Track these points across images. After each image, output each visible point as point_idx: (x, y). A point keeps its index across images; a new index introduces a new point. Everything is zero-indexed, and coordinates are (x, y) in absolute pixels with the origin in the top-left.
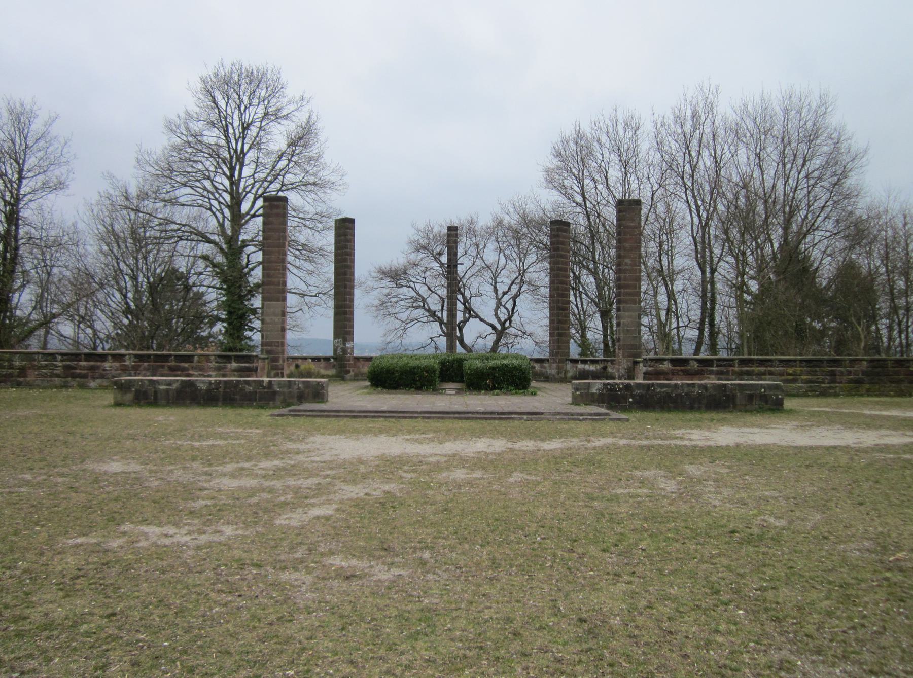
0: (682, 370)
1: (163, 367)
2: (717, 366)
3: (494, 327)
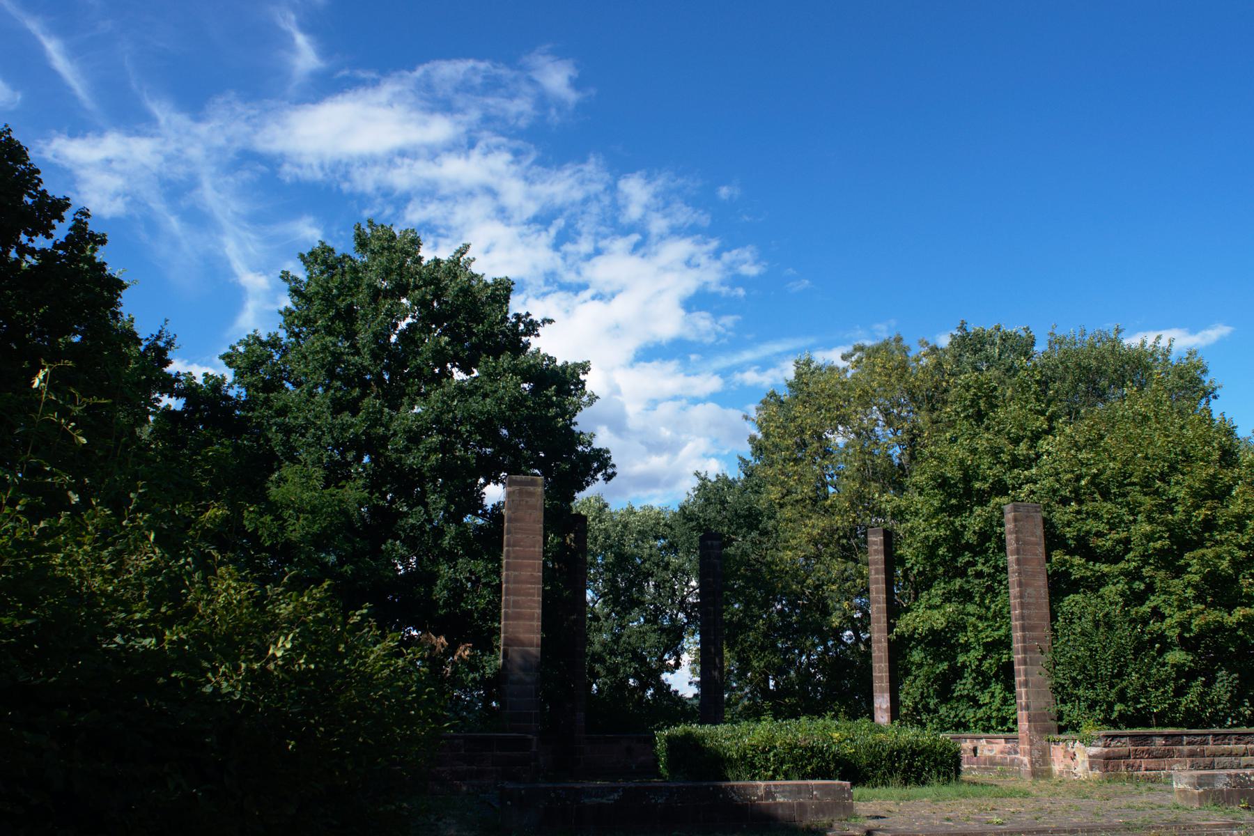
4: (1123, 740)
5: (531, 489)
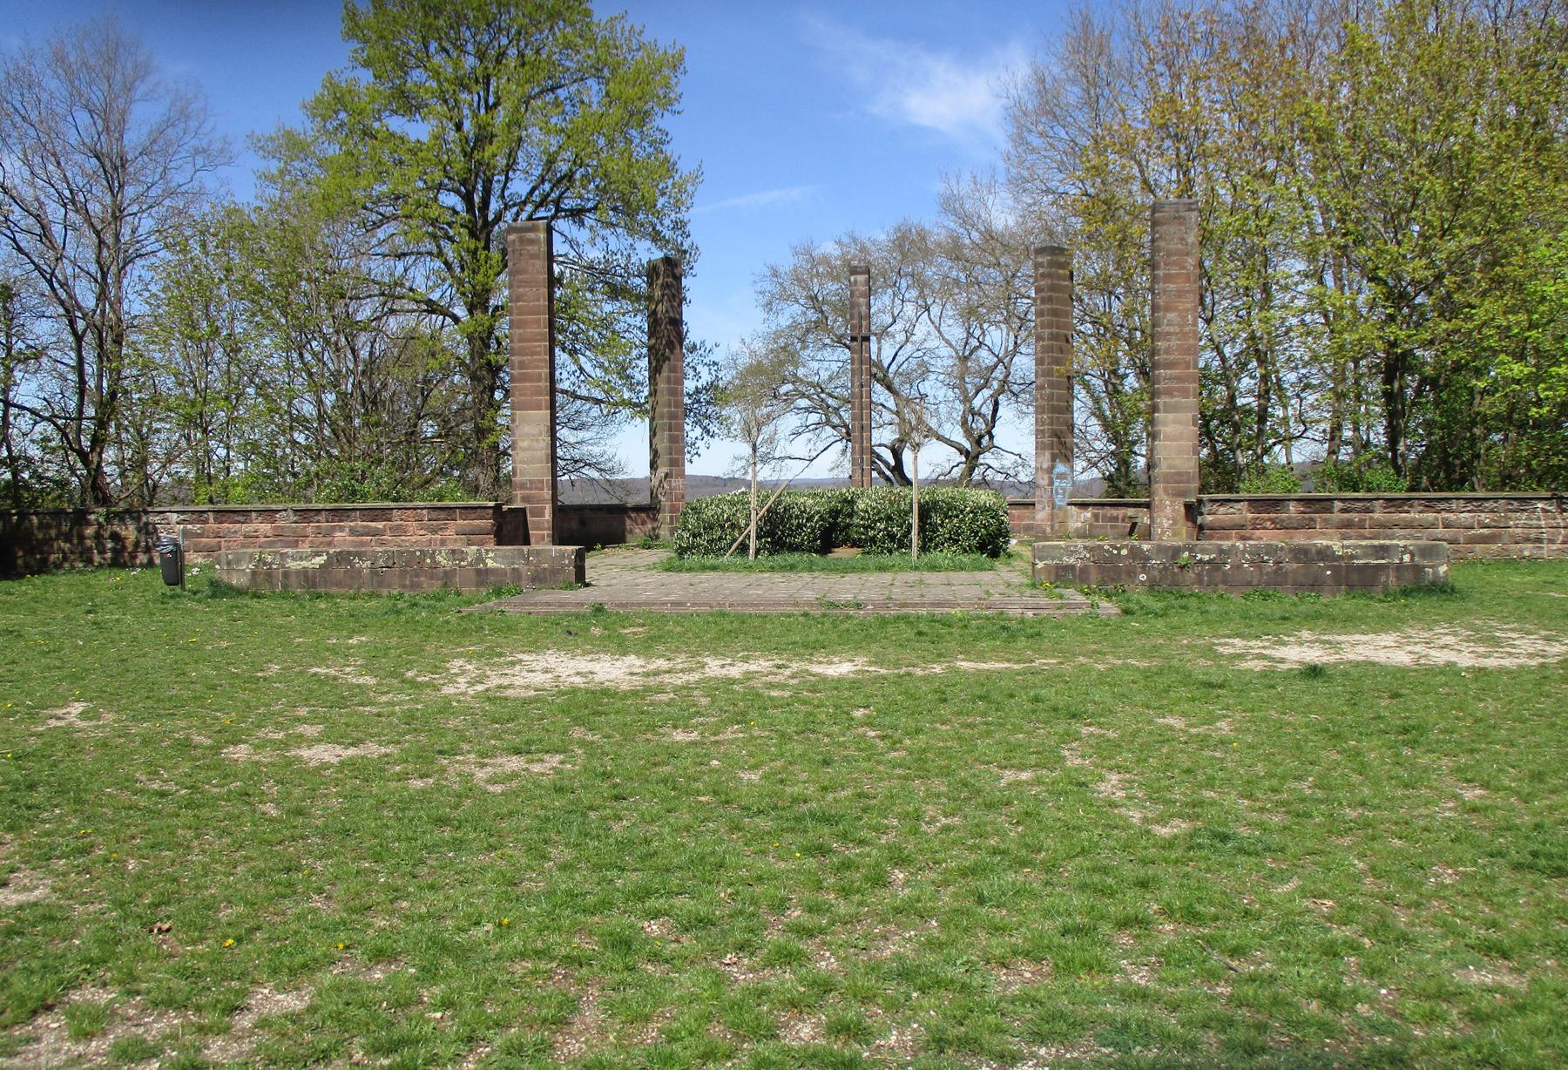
0: (1273, 521)
1: (341, 529)
2: (1343, 511)
3: (961, 450)
4: (1238, 506)
5: (532, 235)
